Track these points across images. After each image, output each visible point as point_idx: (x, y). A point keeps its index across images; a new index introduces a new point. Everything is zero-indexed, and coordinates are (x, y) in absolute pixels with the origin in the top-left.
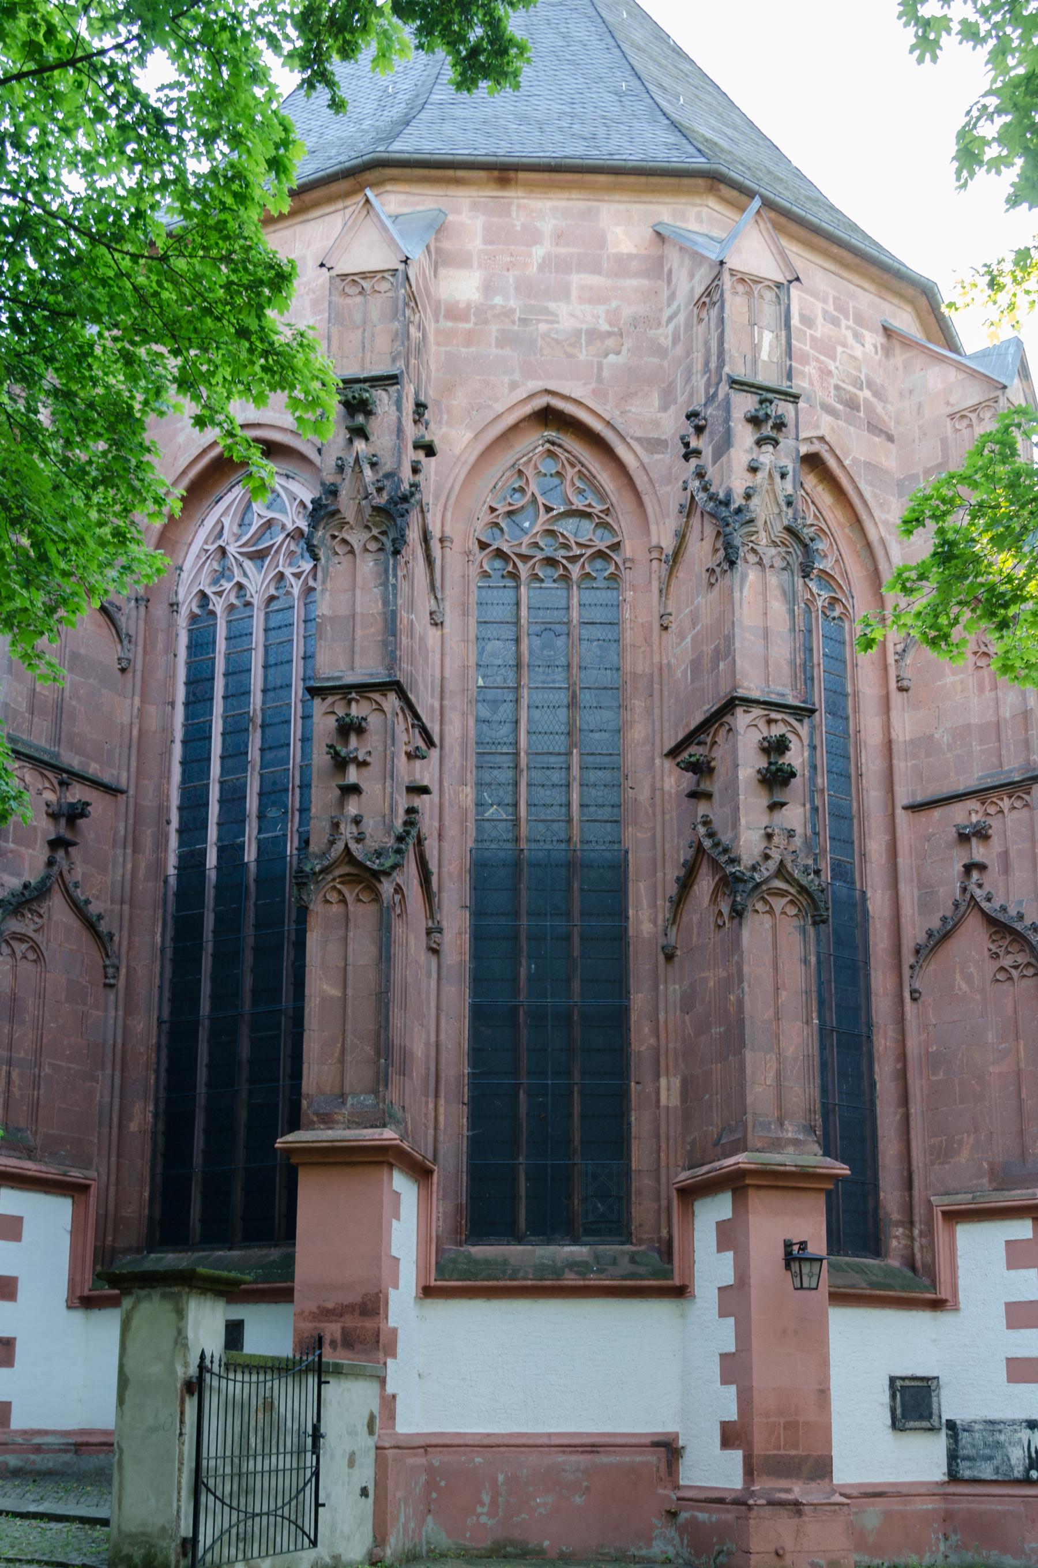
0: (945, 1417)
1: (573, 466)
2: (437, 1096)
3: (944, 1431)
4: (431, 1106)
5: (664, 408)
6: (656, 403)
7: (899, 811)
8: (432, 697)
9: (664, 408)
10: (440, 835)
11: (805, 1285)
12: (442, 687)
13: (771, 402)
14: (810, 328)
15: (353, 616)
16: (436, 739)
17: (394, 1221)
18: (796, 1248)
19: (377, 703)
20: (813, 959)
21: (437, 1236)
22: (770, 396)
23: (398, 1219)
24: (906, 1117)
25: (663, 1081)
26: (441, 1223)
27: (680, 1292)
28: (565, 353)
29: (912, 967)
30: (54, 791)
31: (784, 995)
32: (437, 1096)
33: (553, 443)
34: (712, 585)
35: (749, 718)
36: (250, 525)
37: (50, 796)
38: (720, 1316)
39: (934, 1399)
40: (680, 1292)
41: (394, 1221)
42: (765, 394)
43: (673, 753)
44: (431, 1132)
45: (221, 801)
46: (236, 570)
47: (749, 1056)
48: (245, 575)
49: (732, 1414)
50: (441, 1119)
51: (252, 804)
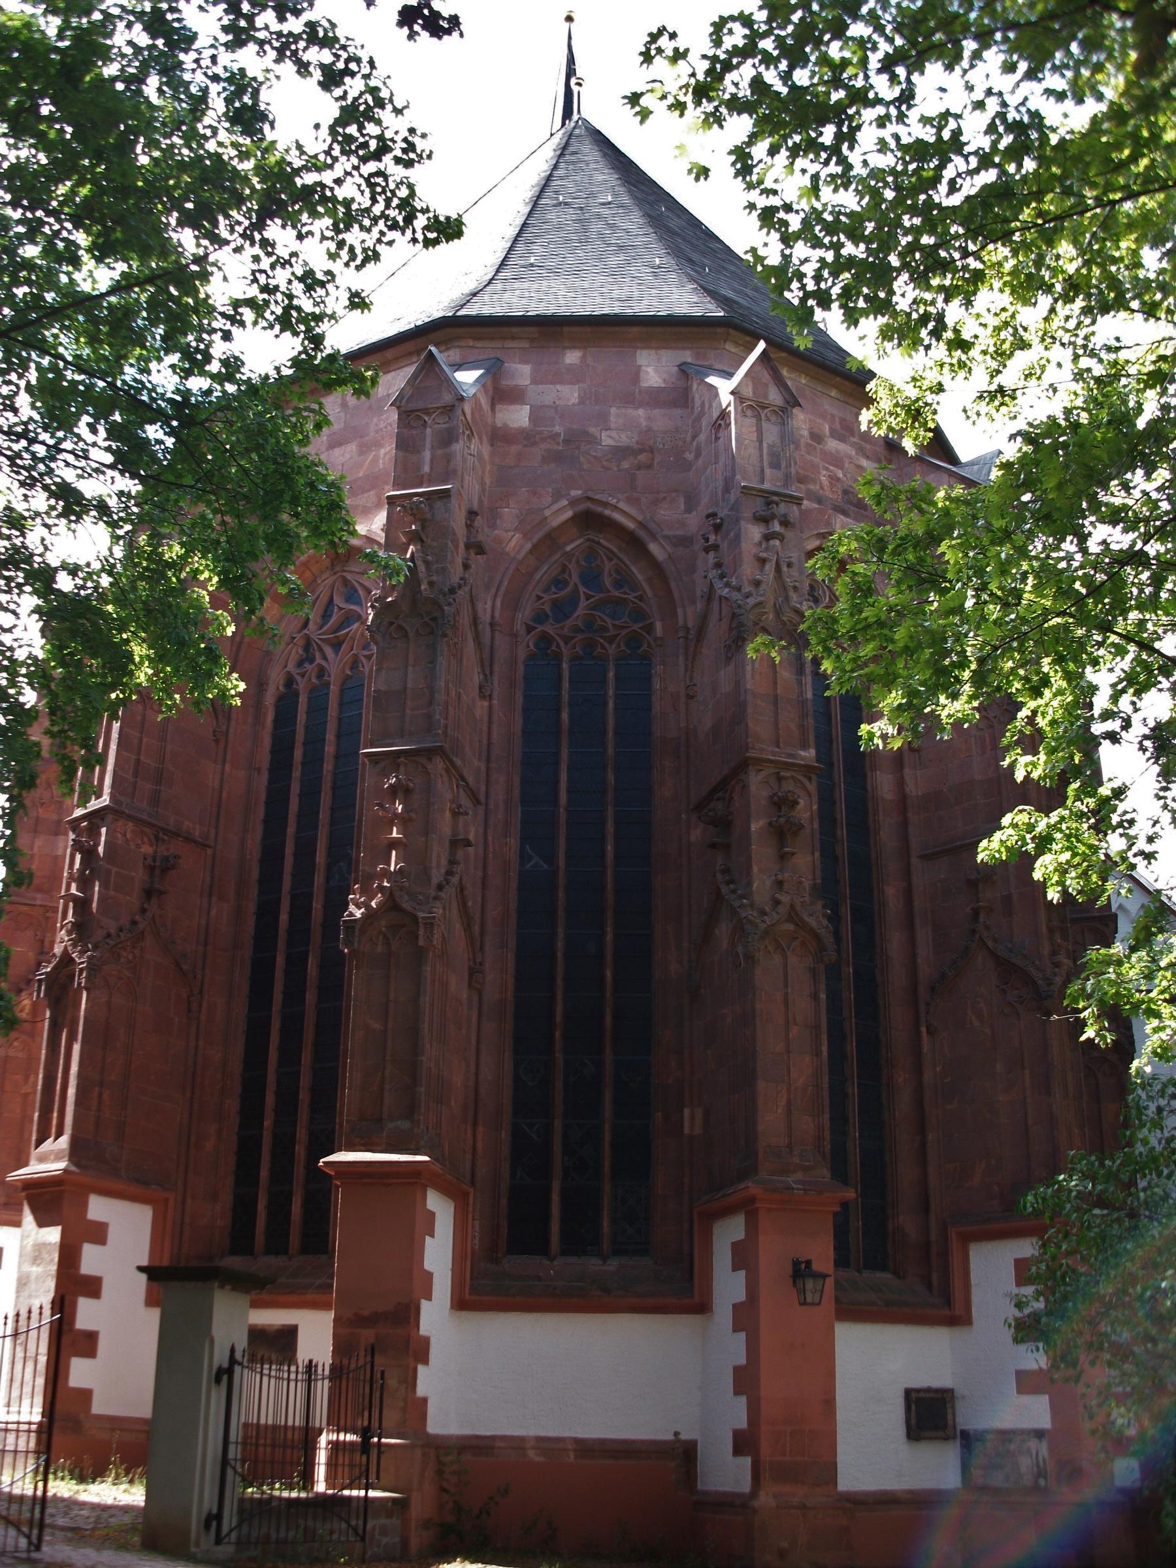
0: (959, 1428)
1: (610, 560)
2: (475, 1125)
3: (958, 1442)
4: (470, 1132)
5: (688, 510)
6: (682, 506)
7: (914, 860)
8: (479, 759)
9: (688, 510)
10: (483, 884)
11: (809, 1300)
12: (489, 752)
13: (777, 504)
14: (819, 443)
15: (405, 689)
16: (482, 798)
17: (428, 1239)
18: (803, 1266)
19: (424, 767)
20: (823, 996)
21: (473, 1253)
22: (775, 498)
23: (433, 1236)
24: (923, 1145)
25: (687, 1112)
26: (477, 1241)
27: (702, 1307)
28: (603, 467)
29: (928, 1004)
30: (151, 846)
31: (794, 1031)
32: (475, 1125)
33: (594, 541)
34: (730, 658)
35: (762, 775)
36: (331, 616)
37: (147, 849)
38: (734, 1331)
39: (949, 1411)
40: (702, 1307)
41: (428, 1239)
42: (769, 499)
43: (698, 808)
44: (469, 1156)
45: (295, 855)
46: (318, 655)
47: (761, 1085)
48: (325, 658)
49: (742, 1423)
50: (480, 1145)
51: (321, 858)
